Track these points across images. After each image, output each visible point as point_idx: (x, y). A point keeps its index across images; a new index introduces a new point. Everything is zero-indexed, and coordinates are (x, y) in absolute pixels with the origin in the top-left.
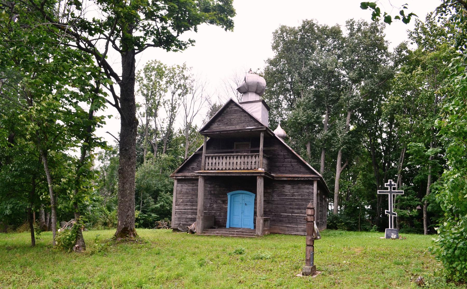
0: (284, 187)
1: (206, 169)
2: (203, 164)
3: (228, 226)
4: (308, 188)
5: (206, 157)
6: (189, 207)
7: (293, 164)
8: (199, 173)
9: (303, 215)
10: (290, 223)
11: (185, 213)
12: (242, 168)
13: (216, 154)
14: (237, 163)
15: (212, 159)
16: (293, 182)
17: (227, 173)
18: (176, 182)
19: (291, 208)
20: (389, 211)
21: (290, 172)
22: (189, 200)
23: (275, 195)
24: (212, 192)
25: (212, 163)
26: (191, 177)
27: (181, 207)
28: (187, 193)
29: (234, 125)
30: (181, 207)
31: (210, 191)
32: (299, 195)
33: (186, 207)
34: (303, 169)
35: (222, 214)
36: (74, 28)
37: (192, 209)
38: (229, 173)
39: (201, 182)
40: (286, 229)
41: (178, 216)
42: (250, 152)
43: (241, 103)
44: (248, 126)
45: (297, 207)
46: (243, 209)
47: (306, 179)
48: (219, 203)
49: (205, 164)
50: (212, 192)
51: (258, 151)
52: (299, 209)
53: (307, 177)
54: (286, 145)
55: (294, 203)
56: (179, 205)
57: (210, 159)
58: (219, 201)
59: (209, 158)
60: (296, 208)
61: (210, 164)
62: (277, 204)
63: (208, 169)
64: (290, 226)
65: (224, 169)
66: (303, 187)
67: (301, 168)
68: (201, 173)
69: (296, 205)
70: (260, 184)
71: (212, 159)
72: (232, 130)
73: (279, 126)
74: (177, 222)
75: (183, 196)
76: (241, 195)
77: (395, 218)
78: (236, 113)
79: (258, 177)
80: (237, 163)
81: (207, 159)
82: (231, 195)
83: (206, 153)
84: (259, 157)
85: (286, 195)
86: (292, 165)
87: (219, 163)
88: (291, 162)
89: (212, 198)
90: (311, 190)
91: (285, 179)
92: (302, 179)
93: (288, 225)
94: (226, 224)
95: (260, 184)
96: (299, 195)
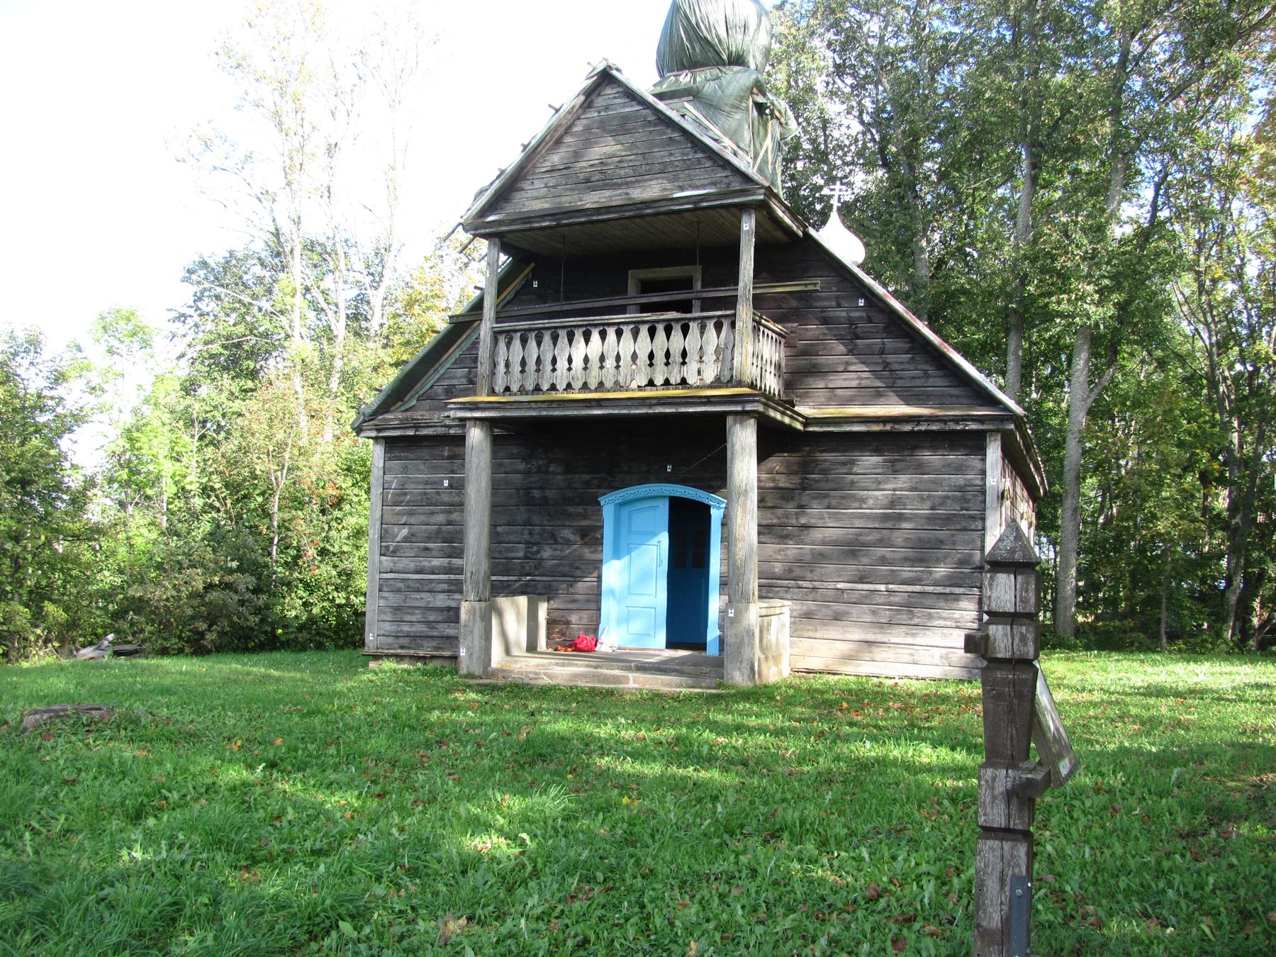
0: (853, 463)
1: (499, 388)
2: (483, 368)
5: (496, 335)
11: (419, 588)
13: (539, 323)
15: (524, 341)
22: (438, 532)
24: (536, 494)
25: (523, 363)
26: (440, 431)
29: (618, 186)
31: (528, 489)
33: (425, 563)
34: (937, 383)
39: (476, 436)
41: (394, 599)
43: (660, 96)
44: (682, 189)
49: (495, 365)
50: (536, 494)
51: (731, 302)
53: (956, 420)
55: (422, 518)
57: (517, 343)
61: (516, 368)
63: (507, 389)
67: (926, 376)
68: (475, 406)
71: (524, 341)
73: (834, 217)
74: (388, 627)
75: (411, 514)
79: (730, 420)
84: (733, 325)
87: (554, 361)
88: (882, 352)
89: (536, 519)
90: (973, 478)
92: (934, 427)
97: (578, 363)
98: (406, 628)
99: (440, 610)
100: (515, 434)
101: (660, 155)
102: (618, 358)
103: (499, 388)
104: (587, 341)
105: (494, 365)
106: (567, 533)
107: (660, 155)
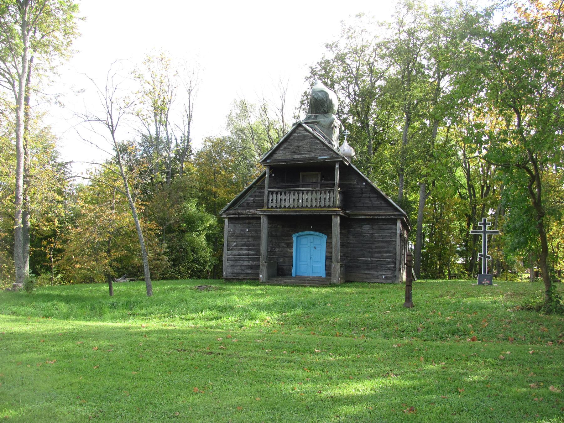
0: (362, 226)
1: (270, 206)
3: (293, 275)
4: (390, 228)
5: (269, 192)
6: (244, 252)
7: (372, 199)
8: (261, 211)
9: (384, 260)
10: (369, 270)
11: (239, 259)
12: (314, 206)
13: (281, 189)
14: (307, 199)
16: (372, 221)
17: (296, 211)
18: (226, 221)
19: (369, 252)
20: (487, 259)
21: (369, 209)
22: (245, 244)
23: (351, 237)
24: (274, 233)
25: (277, 200)
26: (246, 216)
27: (234, 253)
28: (241, 235)
30: (234, 253)
32: (380, 236)
33: (241, 253)
34: (384, 205)
35: (287, 259)
36: (439, 206)
37: (248, 255)
38: (299, 211)
39: (264, 221)
40: (365, 276)
41: (231, 263)
42: (319, 185)
45: (377, 250)
46: (310, 253)
47: (388, 217)
48: (283, 247)
50: (274, 233)
51: (333, 185)
52: (380, 252)
53: (389, 216)
54: (364, 177)
56: (232, 250)
57: (275, 194)
58: (283, 244)
59: (272, 194)
60: (376, 252)
61: (274, 201)
62: (353, 247)
63: (272, 207)
64: (369, 272)
65: (292, 206)
66: (384, 226)
67: (381, 203)
68: (264, 211)
69: (376, 247)
70: (336, 221)
72: (301, 161)
74: (229, 271)
75: (236, 239)
76: (309, 237)
77: (481, 251)
78: (305, 140)
79: (333, 217)
80: (307, 199)
81: (270, 195)
82: (297, 237)
83: (269, 188)
85: (364, 236)
86: (371, 200)
87: (285, 200)
88: (369, 197)
91: (363, 217)
92: (383, 217)
93: (366, 272)
94: (291, 271)
95: (336, 221)
96: (380, 236)
97: (305, 200)
98: (235, 271)
99: (246, 266)
100: (272, 219)
101: (314, 147)
102: (303, 199)
103: (270, 206)
104: (330, 194)
105: (268, 200)
106: (283, 244)
107: (314, 147)
